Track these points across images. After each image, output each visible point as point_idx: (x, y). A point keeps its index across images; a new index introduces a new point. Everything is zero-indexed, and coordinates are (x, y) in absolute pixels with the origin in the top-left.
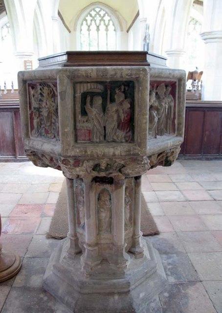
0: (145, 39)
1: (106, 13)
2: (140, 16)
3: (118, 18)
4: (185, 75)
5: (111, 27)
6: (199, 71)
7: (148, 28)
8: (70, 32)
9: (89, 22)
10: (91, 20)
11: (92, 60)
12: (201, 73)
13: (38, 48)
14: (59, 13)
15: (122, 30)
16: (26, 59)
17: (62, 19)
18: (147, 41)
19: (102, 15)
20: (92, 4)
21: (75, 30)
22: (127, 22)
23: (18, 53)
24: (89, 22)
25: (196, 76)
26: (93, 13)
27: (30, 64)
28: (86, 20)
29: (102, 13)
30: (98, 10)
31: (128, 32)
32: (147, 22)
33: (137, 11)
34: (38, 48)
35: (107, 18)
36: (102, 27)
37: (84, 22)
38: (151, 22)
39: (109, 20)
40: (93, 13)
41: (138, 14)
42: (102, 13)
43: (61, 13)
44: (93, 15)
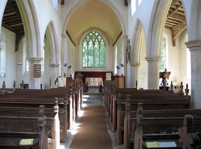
0: (127, 50)
1: (99, 34)
2: (123, 34)
3: (107, 37)
4: (198, 139)
5: (102, 43)
6: (168, 71)
7: (129, 42)
8: (75, 45)
9: (88, 40)
10: (89, 39)
11: (159, 36)
12: (169, 73)
13: (50, 55)
14: (67, 33)
15: (109, 45)
16: (36, 63)
17: (70, 37)
18: (129, 51)
19: (97, 35)
20: (90, 29)
21: (79, 44)
22: (112, 40)
23: (29, 58)
24: (88, 40)
25: (166, 75)
26: (91, 34)
27: (39, 69)
28: (86, 39)
29: (97, 34)
30: (94, 32)
31: (113, 46)
32: (128, 38)
33: (121, 31)
34: (50, 55)
35: (99, 37)
36: (97, 43)
37: (85, 40)
38: (130, 37)
39: (101, 39)
40: (91, 34)
41: (121, 33)
42: (97, 34)
43: (69, 33)
44: (97, 35)
